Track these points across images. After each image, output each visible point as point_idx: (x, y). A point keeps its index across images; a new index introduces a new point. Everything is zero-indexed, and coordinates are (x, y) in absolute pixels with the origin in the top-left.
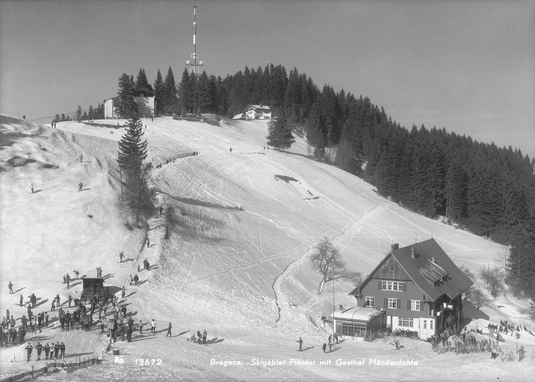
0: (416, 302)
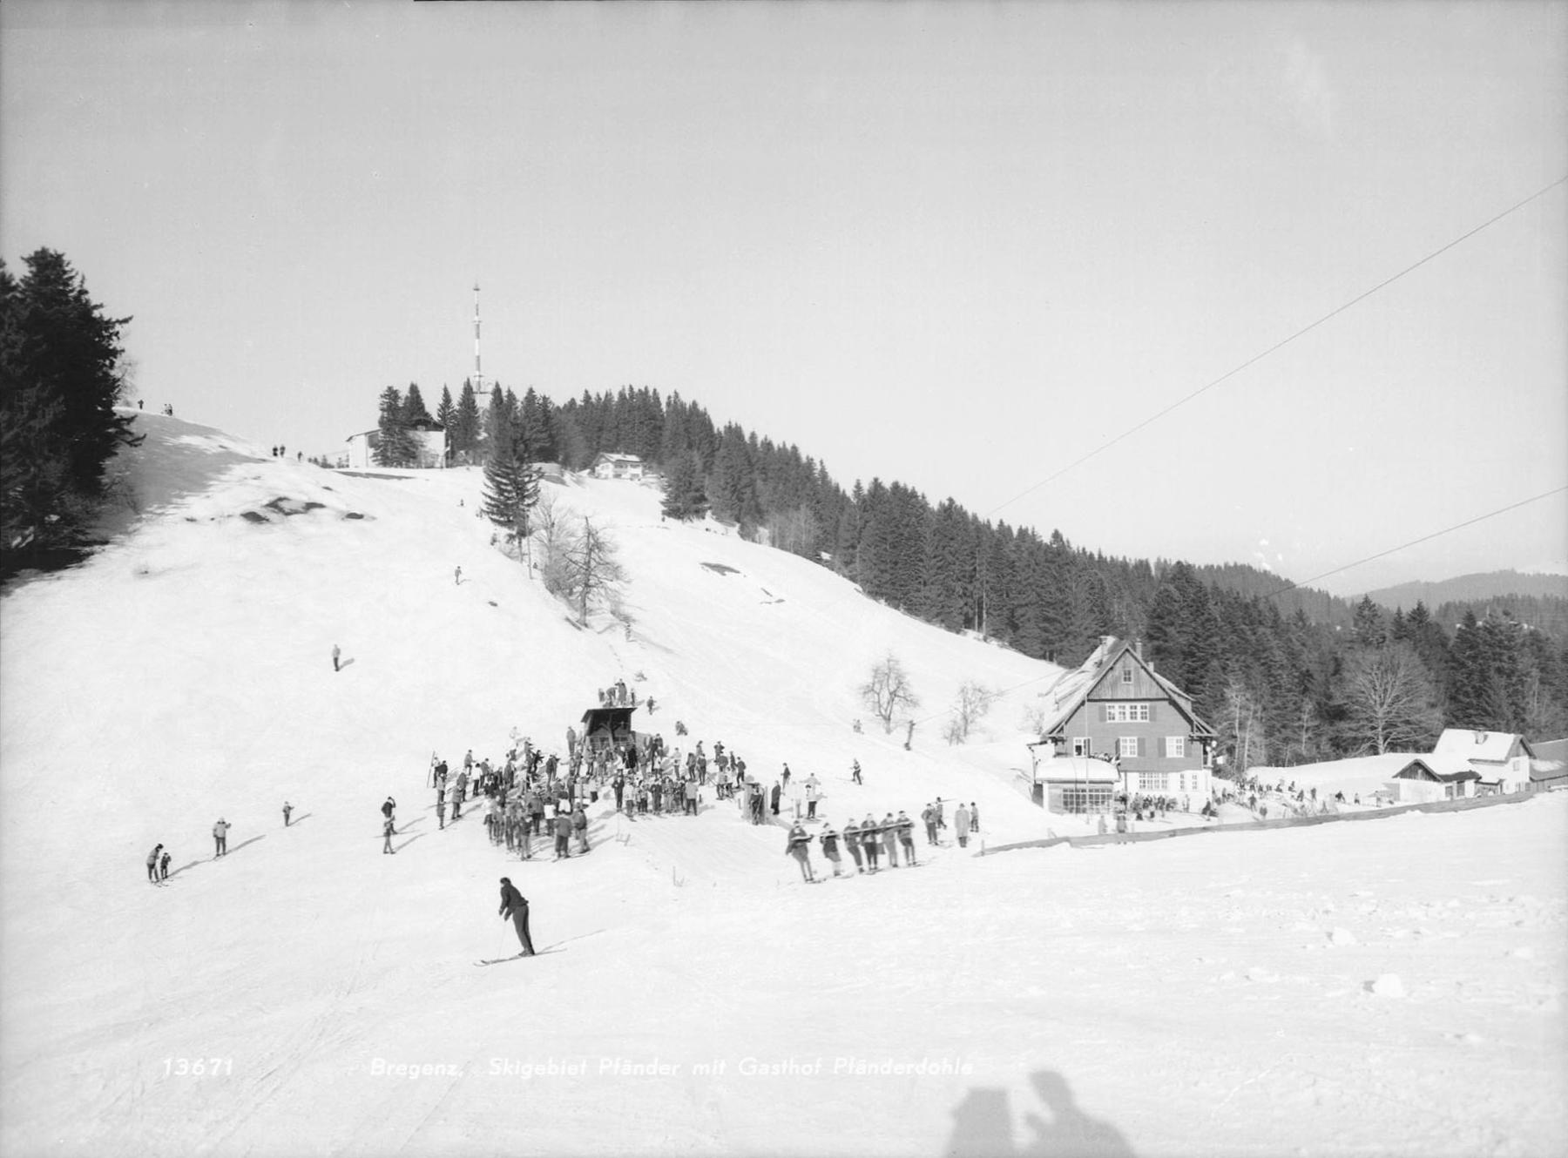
0: (1175, 741)
